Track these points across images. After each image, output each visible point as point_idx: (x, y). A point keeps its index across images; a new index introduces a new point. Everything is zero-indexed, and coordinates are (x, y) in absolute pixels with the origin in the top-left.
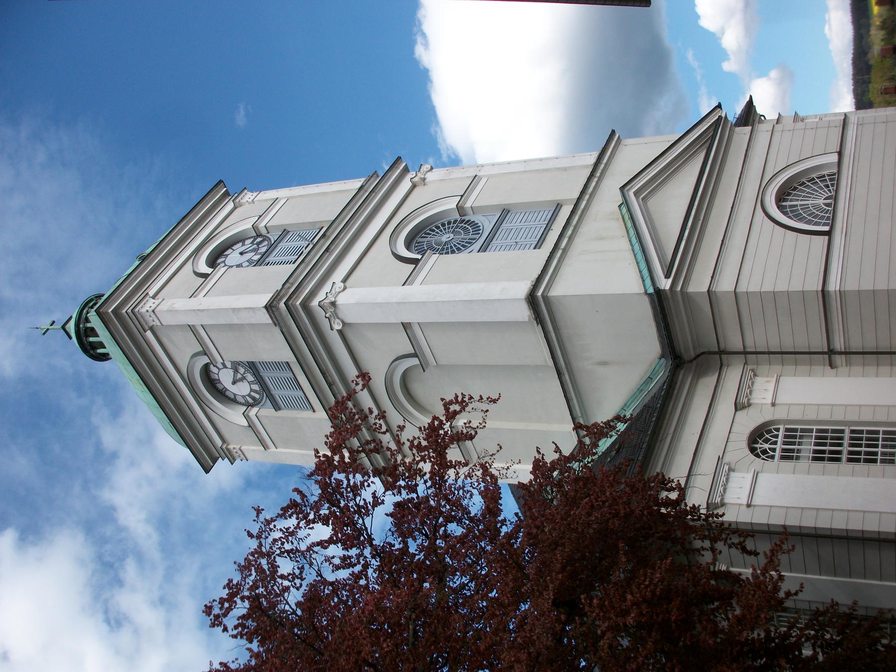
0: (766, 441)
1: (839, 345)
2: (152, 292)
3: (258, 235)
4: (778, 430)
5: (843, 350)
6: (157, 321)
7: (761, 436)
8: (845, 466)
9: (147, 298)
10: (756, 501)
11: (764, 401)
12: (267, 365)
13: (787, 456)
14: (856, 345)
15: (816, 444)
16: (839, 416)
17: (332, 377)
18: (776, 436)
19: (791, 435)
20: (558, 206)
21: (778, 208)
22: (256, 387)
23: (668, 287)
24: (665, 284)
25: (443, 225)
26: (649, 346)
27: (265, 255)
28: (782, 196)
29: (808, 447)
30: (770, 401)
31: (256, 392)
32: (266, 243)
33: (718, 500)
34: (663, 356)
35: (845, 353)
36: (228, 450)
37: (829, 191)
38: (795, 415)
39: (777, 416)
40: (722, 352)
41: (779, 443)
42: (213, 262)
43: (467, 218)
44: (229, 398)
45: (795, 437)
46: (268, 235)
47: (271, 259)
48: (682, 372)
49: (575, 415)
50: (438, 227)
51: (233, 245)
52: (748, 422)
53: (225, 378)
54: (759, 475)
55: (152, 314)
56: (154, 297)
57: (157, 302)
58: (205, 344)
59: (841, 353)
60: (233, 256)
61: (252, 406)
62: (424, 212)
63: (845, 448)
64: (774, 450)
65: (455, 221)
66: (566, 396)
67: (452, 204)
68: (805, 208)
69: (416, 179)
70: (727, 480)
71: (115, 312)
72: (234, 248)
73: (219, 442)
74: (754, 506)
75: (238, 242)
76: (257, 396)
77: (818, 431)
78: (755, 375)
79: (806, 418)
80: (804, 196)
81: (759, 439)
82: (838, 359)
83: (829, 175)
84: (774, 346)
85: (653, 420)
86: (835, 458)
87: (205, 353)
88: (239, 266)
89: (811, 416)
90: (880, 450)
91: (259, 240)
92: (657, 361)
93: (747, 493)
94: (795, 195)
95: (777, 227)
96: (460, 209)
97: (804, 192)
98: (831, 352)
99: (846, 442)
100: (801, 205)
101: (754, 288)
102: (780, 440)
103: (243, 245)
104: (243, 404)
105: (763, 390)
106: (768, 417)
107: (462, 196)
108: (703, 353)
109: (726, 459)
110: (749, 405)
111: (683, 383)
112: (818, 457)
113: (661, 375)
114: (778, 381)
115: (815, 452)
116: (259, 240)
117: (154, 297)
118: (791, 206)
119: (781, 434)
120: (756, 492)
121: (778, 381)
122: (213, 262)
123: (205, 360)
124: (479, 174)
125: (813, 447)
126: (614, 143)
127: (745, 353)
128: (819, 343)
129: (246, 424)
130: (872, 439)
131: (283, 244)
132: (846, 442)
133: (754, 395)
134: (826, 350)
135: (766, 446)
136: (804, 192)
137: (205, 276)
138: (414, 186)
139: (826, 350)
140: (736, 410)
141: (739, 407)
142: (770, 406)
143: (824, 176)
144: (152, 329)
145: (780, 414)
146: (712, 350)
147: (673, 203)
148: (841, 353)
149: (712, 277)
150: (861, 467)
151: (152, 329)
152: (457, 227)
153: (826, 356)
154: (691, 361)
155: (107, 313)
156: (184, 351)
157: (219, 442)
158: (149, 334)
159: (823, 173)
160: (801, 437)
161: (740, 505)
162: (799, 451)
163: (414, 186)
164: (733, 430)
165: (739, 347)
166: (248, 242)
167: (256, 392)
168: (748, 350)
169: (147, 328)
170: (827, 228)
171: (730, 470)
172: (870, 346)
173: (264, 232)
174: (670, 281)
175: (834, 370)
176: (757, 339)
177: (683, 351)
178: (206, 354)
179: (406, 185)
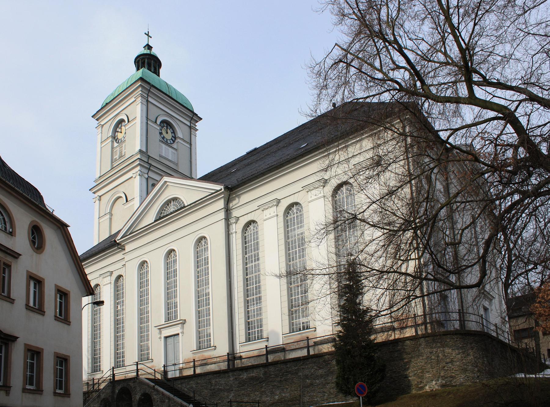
42: (163, 122)
144: (135, 100)
151: (135, 100)
158: (133, 99)
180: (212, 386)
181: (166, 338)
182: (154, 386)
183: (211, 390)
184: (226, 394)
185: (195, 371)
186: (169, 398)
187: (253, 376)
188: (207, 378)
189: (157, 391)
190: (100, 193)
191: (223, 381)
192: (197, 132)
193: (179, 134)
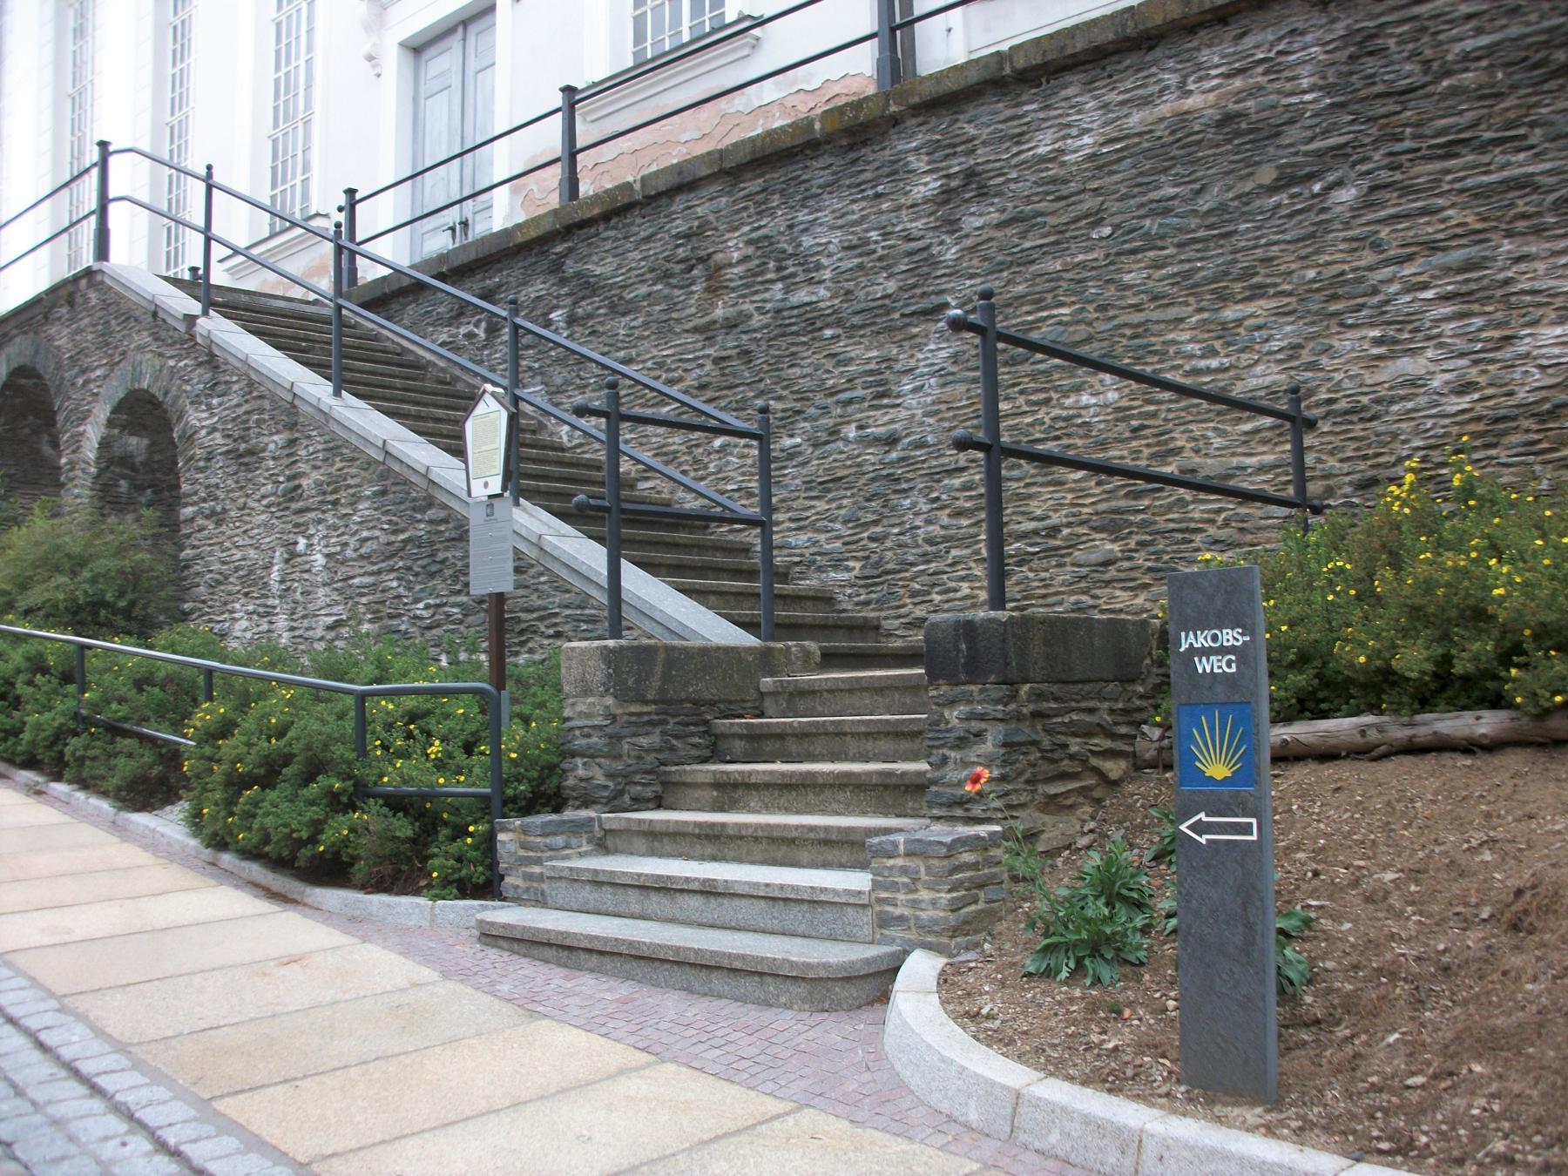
180: (715, 289)
181: (418, 48)
182: (190, 320)
183: (707, 332)
184: (864, 353)
185: (572, 182)
186: (291, 414)
187: (1183, 117)
188: (680, 226)
189: (212, 359)
191: (826, 228)
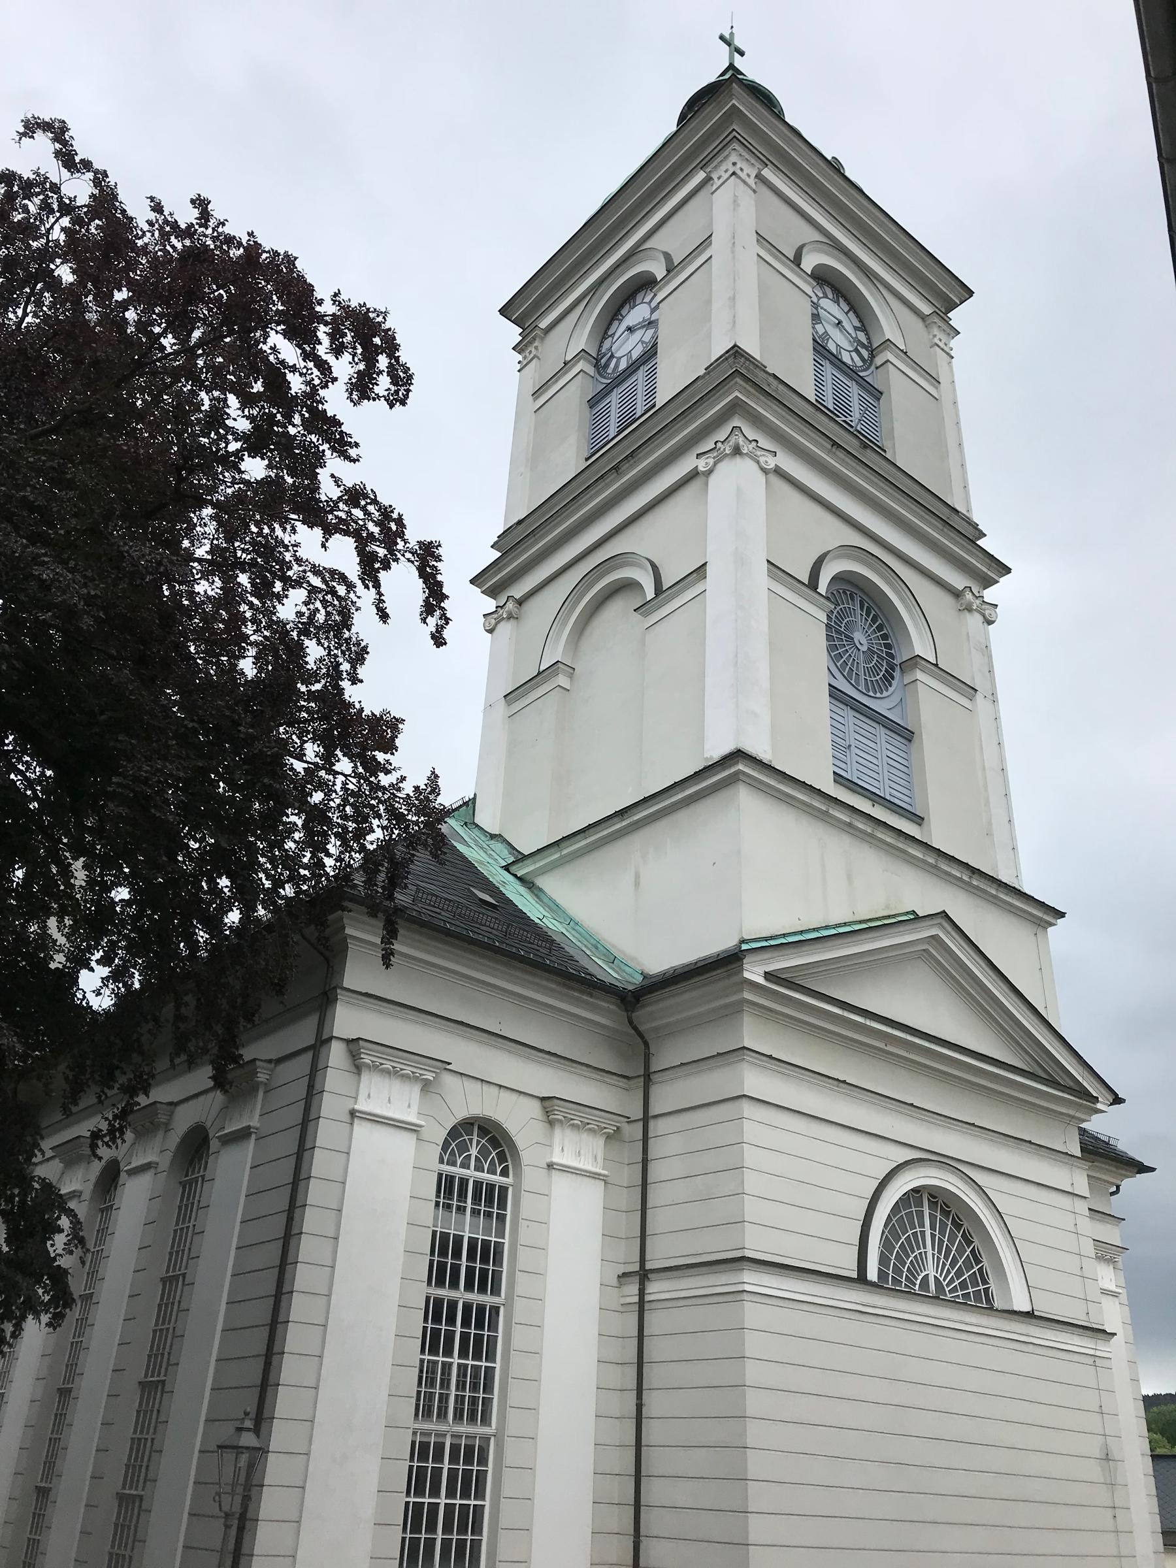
0: (483, 1152)
1: (657, 1289)
2: (767, 173)
3: (871, 350)
4: (504, 1173)
5: (647, 1298)
6: (721, 181)
7: (495, 1143)
8: (420, 1292)
9: (758, 165)
10: (361, 1130)
11: (557, 1149)
12: (652, 373)
13: (448, 1187)
14: (656, 1322)
15: (473, 1243)
16: (523, 1285)
17: (631, 468)
18: (492, 1171)
19: (492, 1199)
20: (918, 820)
21: (916, 1190)
22: (623, 365)
23: (746, 975)
24: (754, 972)
25: (885, 637)
26: (658, 955)
27: (836, 361)
28: (938, 1199)
29: (468, 1228)
30: (555, 1160)
31: (617, 366)
32: (860, 363)
33: (367, 1060)
34: (645, 976)
35: (642, 1303)
36: (534, 339)
37: (954, 1290)
38: (529, 1206)
39: (527, 1172)
40: (648, 1079)
41: (479, 1174)
42: (822, 277)
43: (897, 674)
44: (608, 328)
45: (490, 1202)
46: (873, 368)
47: (828, 369)
48: (612, 1007)
49: (563, 845)
50: (880, 628)
51: (855, 312)
52: (519, 1120)
53: (637, 314)
54: (414, 1136)
55: (730, 172)
56: (759, 177)
57: (751, 181)
58: (684, 269)
59: (642, 1293)
60: (832, 308)
61: (596, 366)
62: (907, 607)
63: (461, 1296)
64: (465, 1165)
65: (892, 657)
66: (590, 826)
67: (921, 646)
68: (917, 1241)
69: (969, 596)
70: (405, 1077)
71: (734, 112)
72: (851, 314)
73: (544, 324)
74: (352, 1124)
75: (861, 321)
76: (609, 371)
77: (499, 1247)
78: (609, 1137)
79: (523, 1224)
80: (941, 1242)
81: (491, 1137)
82: (633, 1289)
83: (986, 1290)
84: (657, 1171)
85: (510, 946)
86: (440, 1275)
87: (671, 269)
88: (816, 318)
89: (525, 1235)
90: (456, 1360)
91: (865, 353)
92: (638, 968)
93: (378, 1111)
94: (943, 1226)
95: (876, 1184)
96: (916, 661)
97: (952, 1240)
98: (644, 1275)
99: (475, 1297)
100: (923, 1233)
101: (751, 1131)
102: (485, 1176)
103: (856, 328)
104: (599, 350)
105: (578, 1150)
106: (526, 1156)
107: (936, 665)
108: (646, 1044)
109: (449, 1080)
110: (551, 1123)
111: (594, 1008)
112: (443, 1244)
113: (611, 974)
114: (594, 1176)
115: (458, 1240)
116: (865, 353)
117: (759, 177)
118: (920, 1215)
119: (497, 1179)
120: (379, 1127)
121: (594, 1176)
122: (822, 277)
123: (659, 272)
124: (979, 697)
125: (467, 1235)
126: (1040, 914)
127: (646, 1119)
128: (661, 1253)
129: (568, 358)
130: (482, 1348)
131: (855, 390)
132: (475, 1297)
133: (568, 1132)
134: (649, 1266)
135: (474, 1152)
136: (952, 1240)
137: (797, 261)
138: (957, 594)
139: (649, 1266)
140: (543, 1099)
141: (547, 1103)
142: (548, 1160)
143: (985, 1282)
144: (708, 180)
145: (531, 1176)
146: (653, 1060)
147: (921, 1004)
148: (642, 1293)
149: (770, 1057)
150: (416, 1323)
151: (708, 180)
152: (882, 658)
153: (636, 1267)
154: (631, 1022)
155: (731, 97)
156: (674, 240)
157: (544, 324)
158: (701, 176)
159: (991, 1281)
160: (488, 1215)
161: (356, 1098)
162: (461, 1210)
163: (957, 594)
164: (505, 1094)
165: (655, 1109)
166: (862, 336)
167: (617, 366)
168: (652, 1124)
169: (708, 170)
170: (872, 1274)
171: (426, 1086)
172: (655, 1349)
173: (879, 360)
174: (761, 980)
175: (615, 1282)
176: (669, 1141)
177: (649, 1009)
178: (669, 271)
179: (958, 580)
190: (518, 591)
192: (953, 343)
193: (81, 1217)
